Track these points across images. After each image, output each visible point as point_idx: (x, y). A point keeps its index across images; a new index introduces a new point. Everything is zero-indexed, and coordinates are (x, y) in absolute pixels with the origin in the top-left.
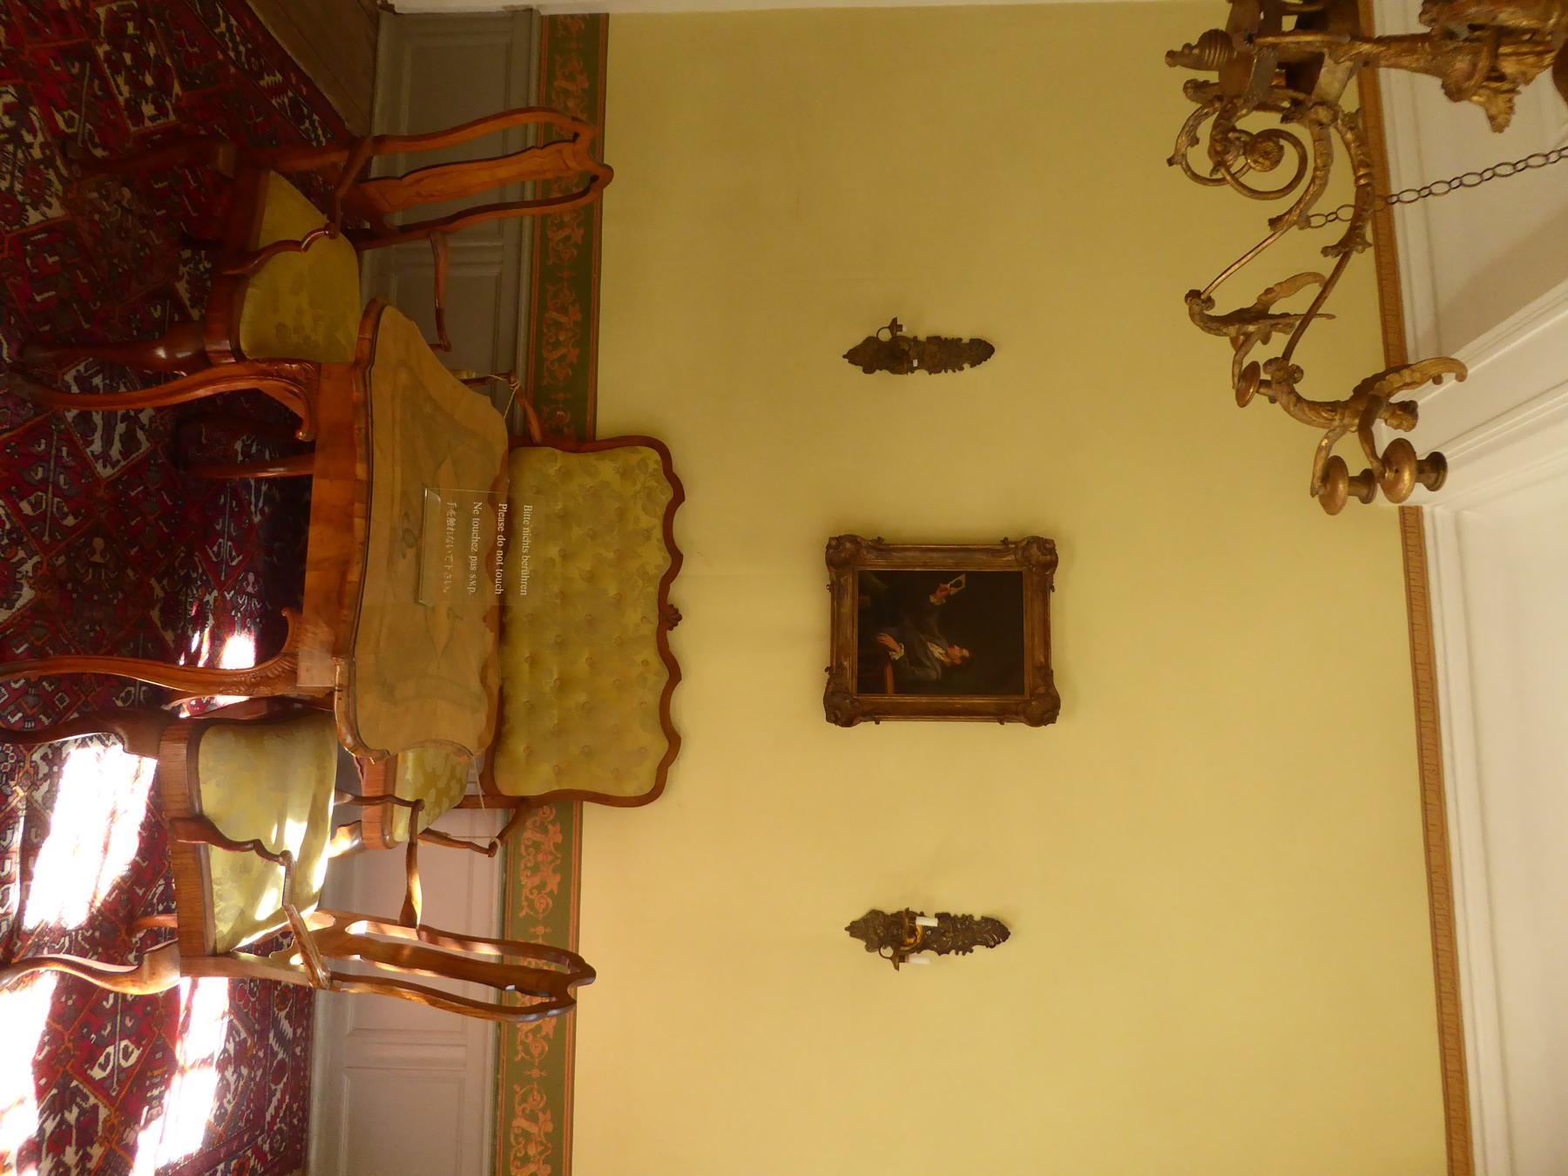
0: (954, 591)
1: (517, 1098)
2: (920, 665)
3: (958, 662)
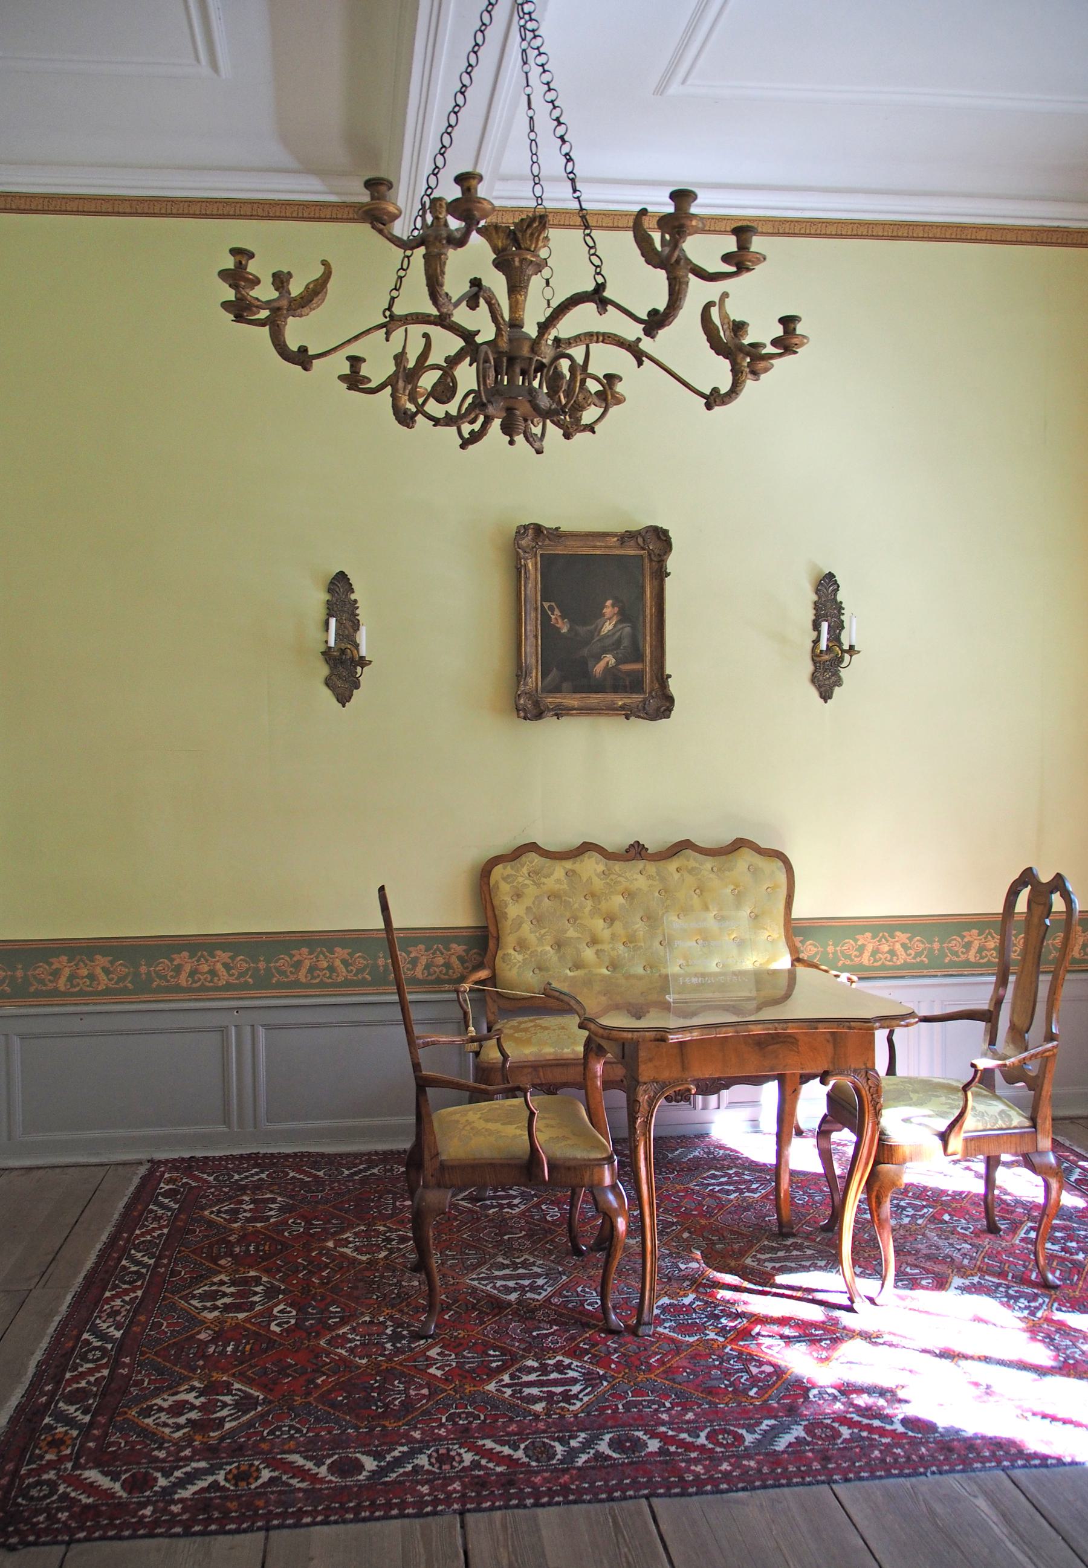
0: (557, 612)
1: (955, 959)
2: (619, 641)
3: (616, 609)
